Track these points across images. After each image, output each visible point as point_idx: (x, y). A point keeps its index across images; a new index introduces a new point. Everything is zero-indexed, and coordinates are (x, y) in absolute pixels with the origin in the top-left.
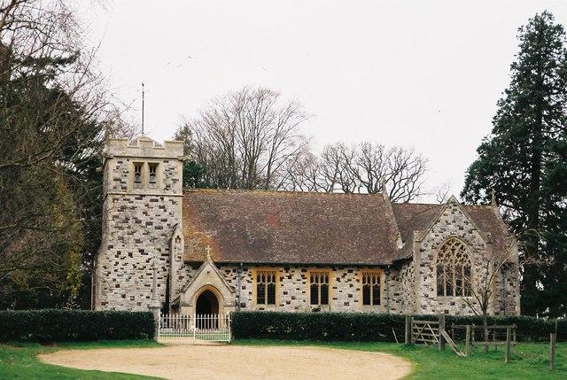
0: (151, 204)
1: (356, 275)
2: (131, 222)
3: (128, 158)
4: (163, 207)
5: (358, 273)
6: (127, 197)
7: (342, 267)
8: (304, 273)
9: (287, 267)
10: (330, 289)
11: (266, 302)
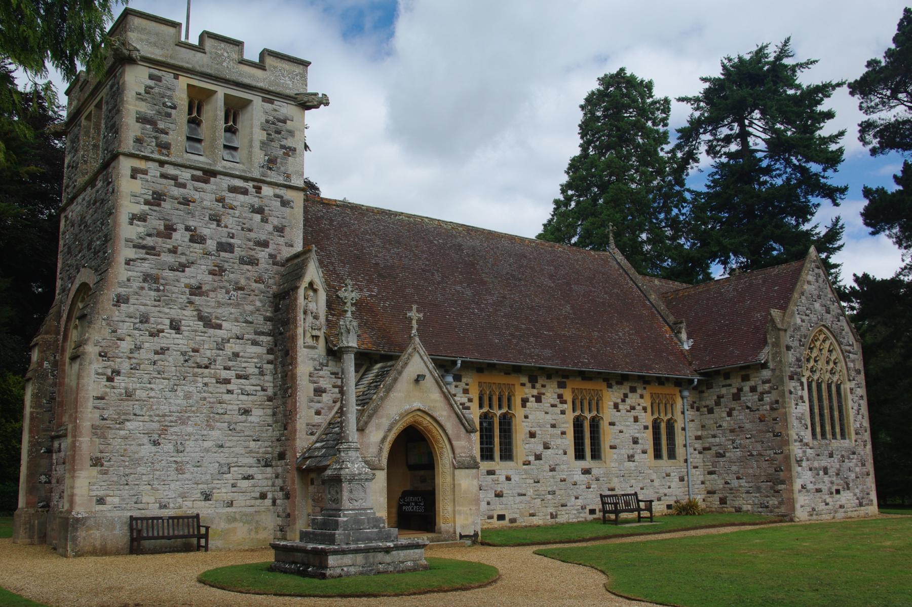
0: (231, 198)
1: (642, 397)
2: (180, 237)
3: (179, 70)
4: (260, 211)
5: (644, 392)
6: (170, 170)
7: (623, 379)
8: (560, 391)
9: (534, 375)
10: (604, 425)
11: (497, 454)
